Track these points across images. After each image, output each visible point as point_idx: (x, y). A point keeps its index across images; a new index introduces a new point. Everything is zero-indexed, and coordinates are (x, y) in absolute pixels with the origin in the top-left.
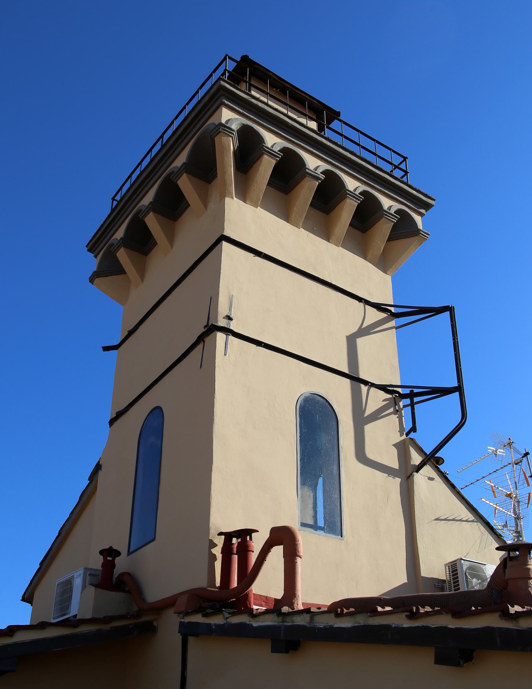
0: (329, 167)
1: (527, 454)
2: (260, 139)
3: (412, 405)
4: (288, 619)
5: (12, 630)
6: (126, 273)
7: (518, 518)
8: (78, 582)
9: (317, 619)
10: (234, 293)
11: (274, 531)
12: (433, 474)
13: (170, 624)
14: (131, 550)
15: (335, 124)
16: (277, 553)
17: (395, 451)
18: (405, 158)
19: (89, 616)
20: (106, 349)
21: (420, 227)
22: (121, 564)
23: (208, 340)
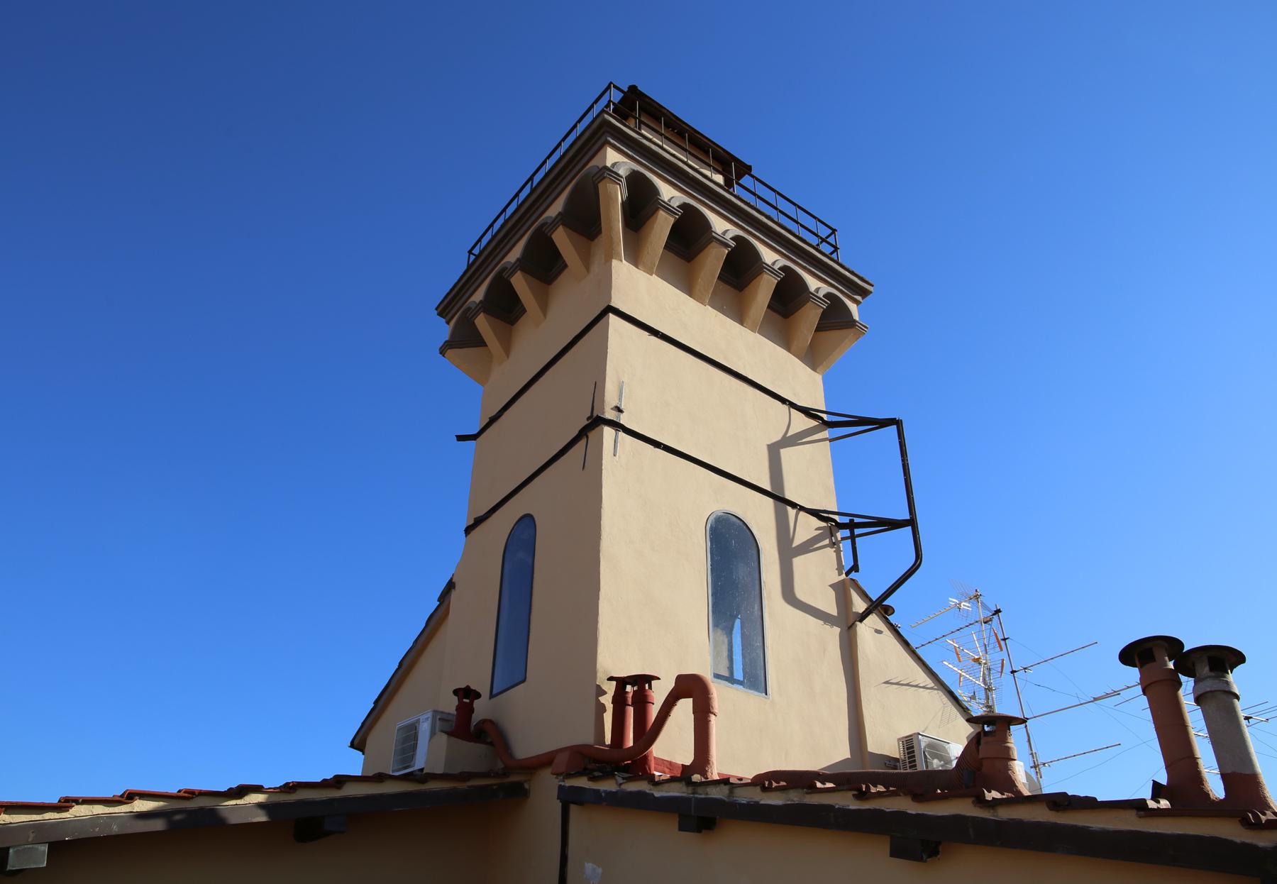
0: (741, 233)
1: (998, 611)
2: (655, 191)
3: (853, 538)
4: (700, 790)
5: (339, 781)
6: (486, 345)
7: (988, 689)
8: (425, 728)
9: (738, 791)
10: (625, 380)
11: (680, 679)
12: (881, 625)
13: (546, 787)
14: (495, 692)
15: (747, 180)
16: (685, 707)
17: (832, 594)
18: (834, 231)
19: (440, 771)
20: (461, 438)
21: (856, 317)
22: (481, 708)
23: (592, 435)
